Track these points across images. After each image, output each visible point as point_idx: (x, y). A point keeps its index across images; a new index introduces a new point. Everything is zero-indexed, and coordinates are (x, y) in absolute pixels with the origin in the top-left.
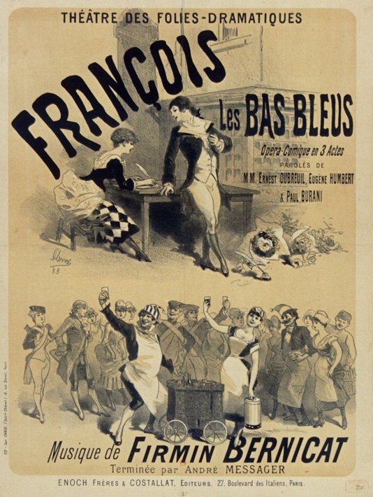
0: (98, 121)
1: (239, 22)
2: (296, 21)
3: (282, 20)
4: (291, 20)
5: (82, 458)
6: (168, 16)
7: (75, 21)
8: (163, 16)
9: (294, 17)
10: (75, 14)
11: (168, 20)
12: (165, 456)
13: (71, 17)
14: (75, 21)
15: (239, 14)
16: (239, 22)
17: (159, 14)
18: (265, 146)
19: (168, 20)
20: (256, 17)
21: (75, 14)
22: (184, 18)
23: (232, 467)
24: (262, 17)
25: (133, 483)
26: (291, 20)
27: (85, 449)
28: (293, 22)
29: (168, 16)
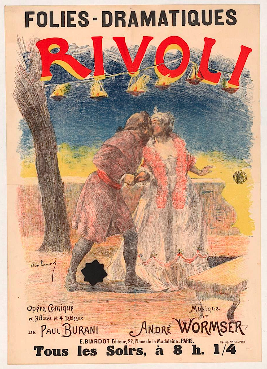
0: (164, 331)
1: (142, 25)
2: (80, 23)
3: (207, 20)
4: (220, 21)
5: (65, 310)
6: (42, 17)
7: (97, 343)
8: (34, 17)
9: (224, 15)
10: (95, 343)
11: (42, 22)
12: (165, 330)
13: (122, 19)
14: (97, 343)
15: (143, 13)
16: (142, 25)
17: (27, 14)
18: (183, 146)
19: (42, 22)
20: (169, 17)
21: (95, 343)
22: (148, 18)
23: (195, 307)
24: (179, 17)
25: (142, 342)
26: (220, 21)
27: (65, 307)
28: (222, 24)
29: (42, 17)
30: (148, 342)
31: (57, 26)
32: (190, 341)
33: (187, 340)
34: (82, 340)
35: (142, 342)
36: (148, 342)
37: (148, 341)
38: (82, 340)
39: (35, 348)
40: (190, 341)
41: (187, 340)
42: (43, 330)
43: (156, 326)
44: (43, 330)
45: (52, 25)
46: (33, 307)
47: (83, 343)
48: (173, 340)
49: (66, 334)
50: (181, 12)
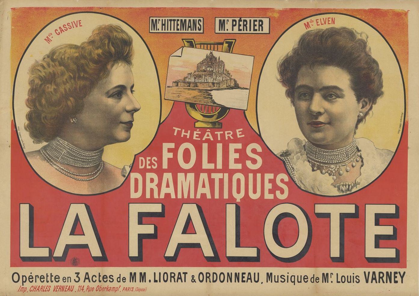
30: (119, 280)
31: (323, 24)
32: (355, 279)
33: (381, 275)
34: (81, 21)
35: (94, 279)
36: (119, 280)
37: (120, 278)
38: (81, 21)
39: (76, 273)
40: (355, 279)
41: (381, 275)
42: (161, 121)
43: (317, 19)
44: (161, 121)
45: (322, 24)
46: (23, 276)
47: (150, 281)
48: (355, 276)
49: (233, 30)
50: (331, 18)
